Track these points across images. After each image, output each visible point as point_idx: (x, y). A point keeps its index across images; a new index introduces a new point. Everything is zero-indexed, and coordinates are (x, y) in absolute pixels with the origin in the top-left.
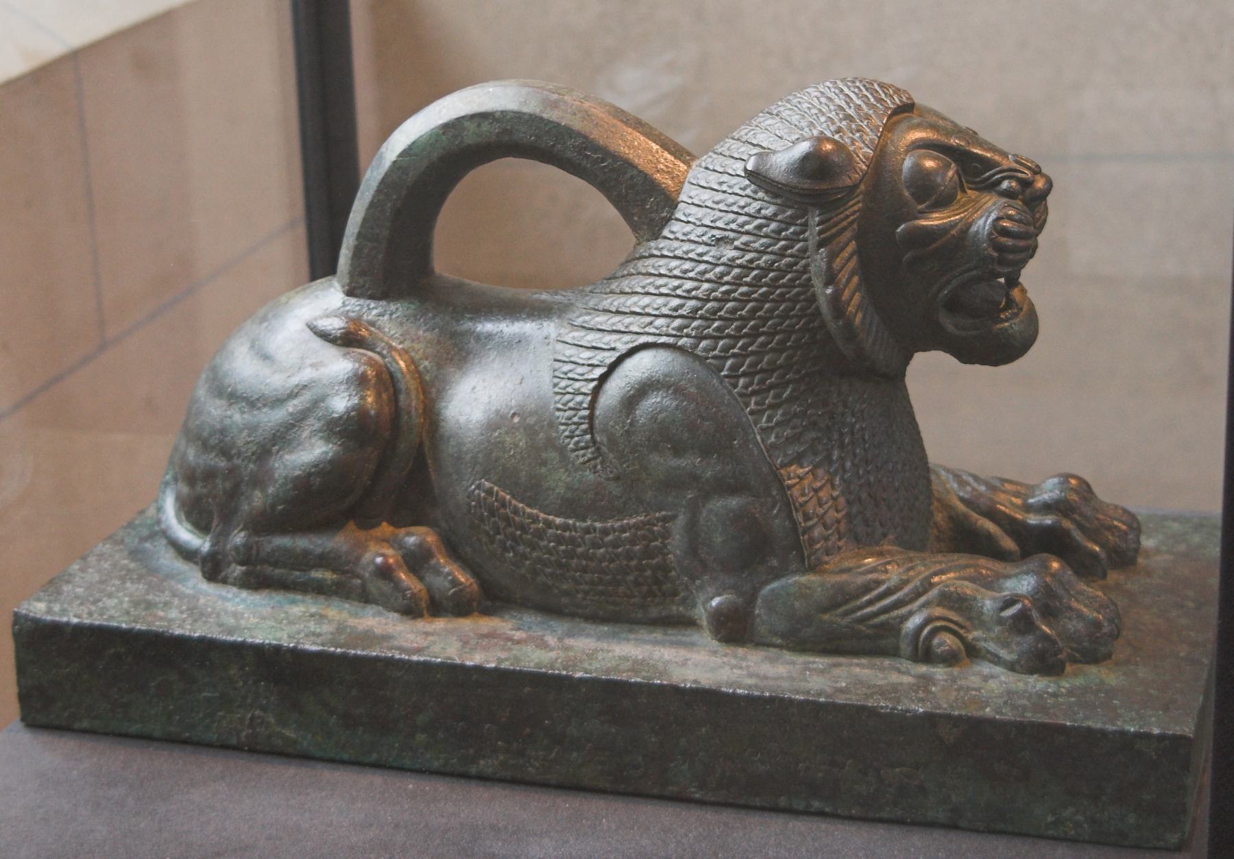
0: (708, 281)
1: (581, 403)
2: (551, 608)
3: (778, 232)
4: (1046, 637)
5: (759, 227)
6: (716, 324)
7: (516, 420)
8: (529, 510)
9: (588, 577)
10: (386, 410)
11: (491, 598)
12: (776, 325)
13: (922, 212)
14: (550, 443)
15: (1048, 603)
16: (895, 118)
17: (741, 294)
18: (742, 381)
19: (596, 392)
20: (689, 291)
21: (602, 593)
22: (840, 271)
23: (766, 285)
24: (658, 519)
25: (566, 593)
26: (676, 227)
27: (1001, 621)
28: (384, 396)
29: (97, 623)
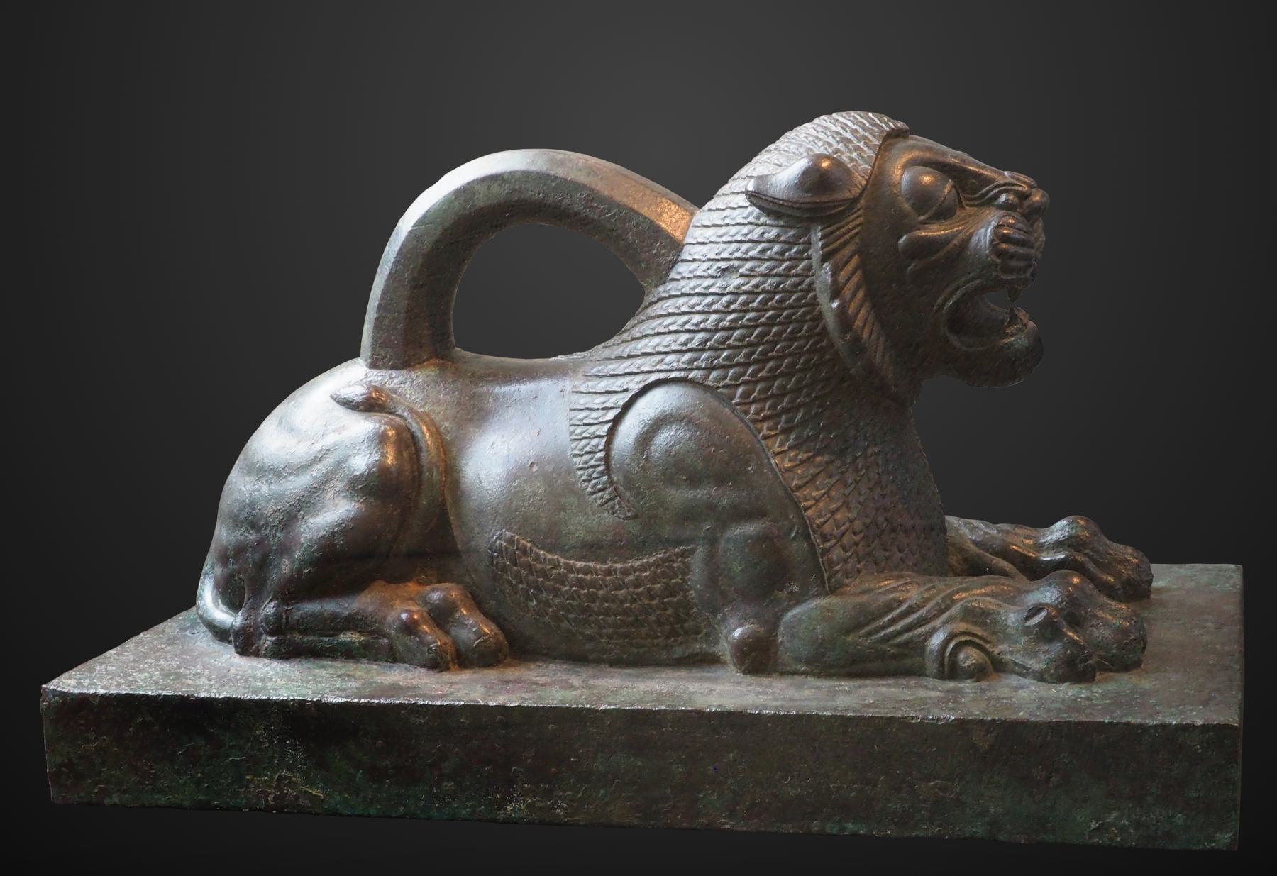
0: (715, 312)
1: (597, 446)
2: (577, 658)
3: (782, 253)
4: (1075, 643)
5: (763, 251)
6: (725, 354)
7: (535, 469)
8: (549, 556)
9: (610, 619)
11: (514, 648)
12: (783, 349)
13: (923, 223)
14: (570, 488)
15: (1072, 614)
16: (889, 141)
17: (749, 320)
18: (753, 408)
19: (611, 433)
20: (697, 324)
21: (626, 635)
22: (845, 284)
23: (773, 308)
24: (677, 555)
25: (591, 638)
26: (683, 269)
27: (1027, 631)
28: (405, 454)
29: (124, 692)
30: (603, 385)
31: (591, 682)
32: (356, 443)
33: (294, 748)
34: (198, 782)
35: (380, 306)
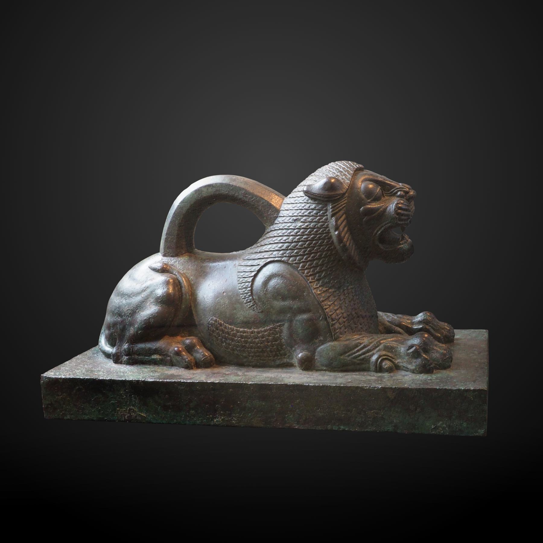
0: (292, 235)
2: (240, 364)
3: (317, 214)
4: (426, 359)
5: (310, 213)
7: (225, 294)
8: (230, 327)
9: (253, 350)
10: (177, 293)
11: (217, 361)
12: (317, 249)
14: (238, 301)
18: (306, 271)
19: (253, 281)
20: (285, 240)
21: (259, 356)
22: (340, 225)
23: (313, 234)
25: (246, 357)
26: (280, 219)
27: (408, 354)
28: (176, 289)
30: (250, 263)
31: (246, 373)
32: (158, 284)
33: (135, 398)
34: (99, 411)
35: (167, 234)
